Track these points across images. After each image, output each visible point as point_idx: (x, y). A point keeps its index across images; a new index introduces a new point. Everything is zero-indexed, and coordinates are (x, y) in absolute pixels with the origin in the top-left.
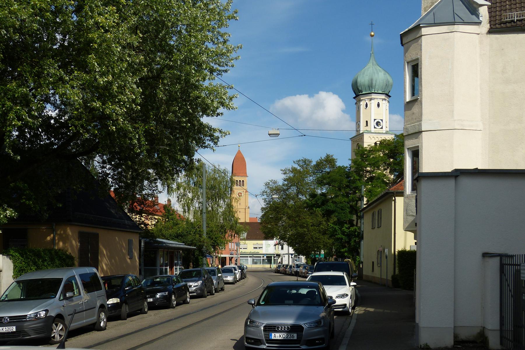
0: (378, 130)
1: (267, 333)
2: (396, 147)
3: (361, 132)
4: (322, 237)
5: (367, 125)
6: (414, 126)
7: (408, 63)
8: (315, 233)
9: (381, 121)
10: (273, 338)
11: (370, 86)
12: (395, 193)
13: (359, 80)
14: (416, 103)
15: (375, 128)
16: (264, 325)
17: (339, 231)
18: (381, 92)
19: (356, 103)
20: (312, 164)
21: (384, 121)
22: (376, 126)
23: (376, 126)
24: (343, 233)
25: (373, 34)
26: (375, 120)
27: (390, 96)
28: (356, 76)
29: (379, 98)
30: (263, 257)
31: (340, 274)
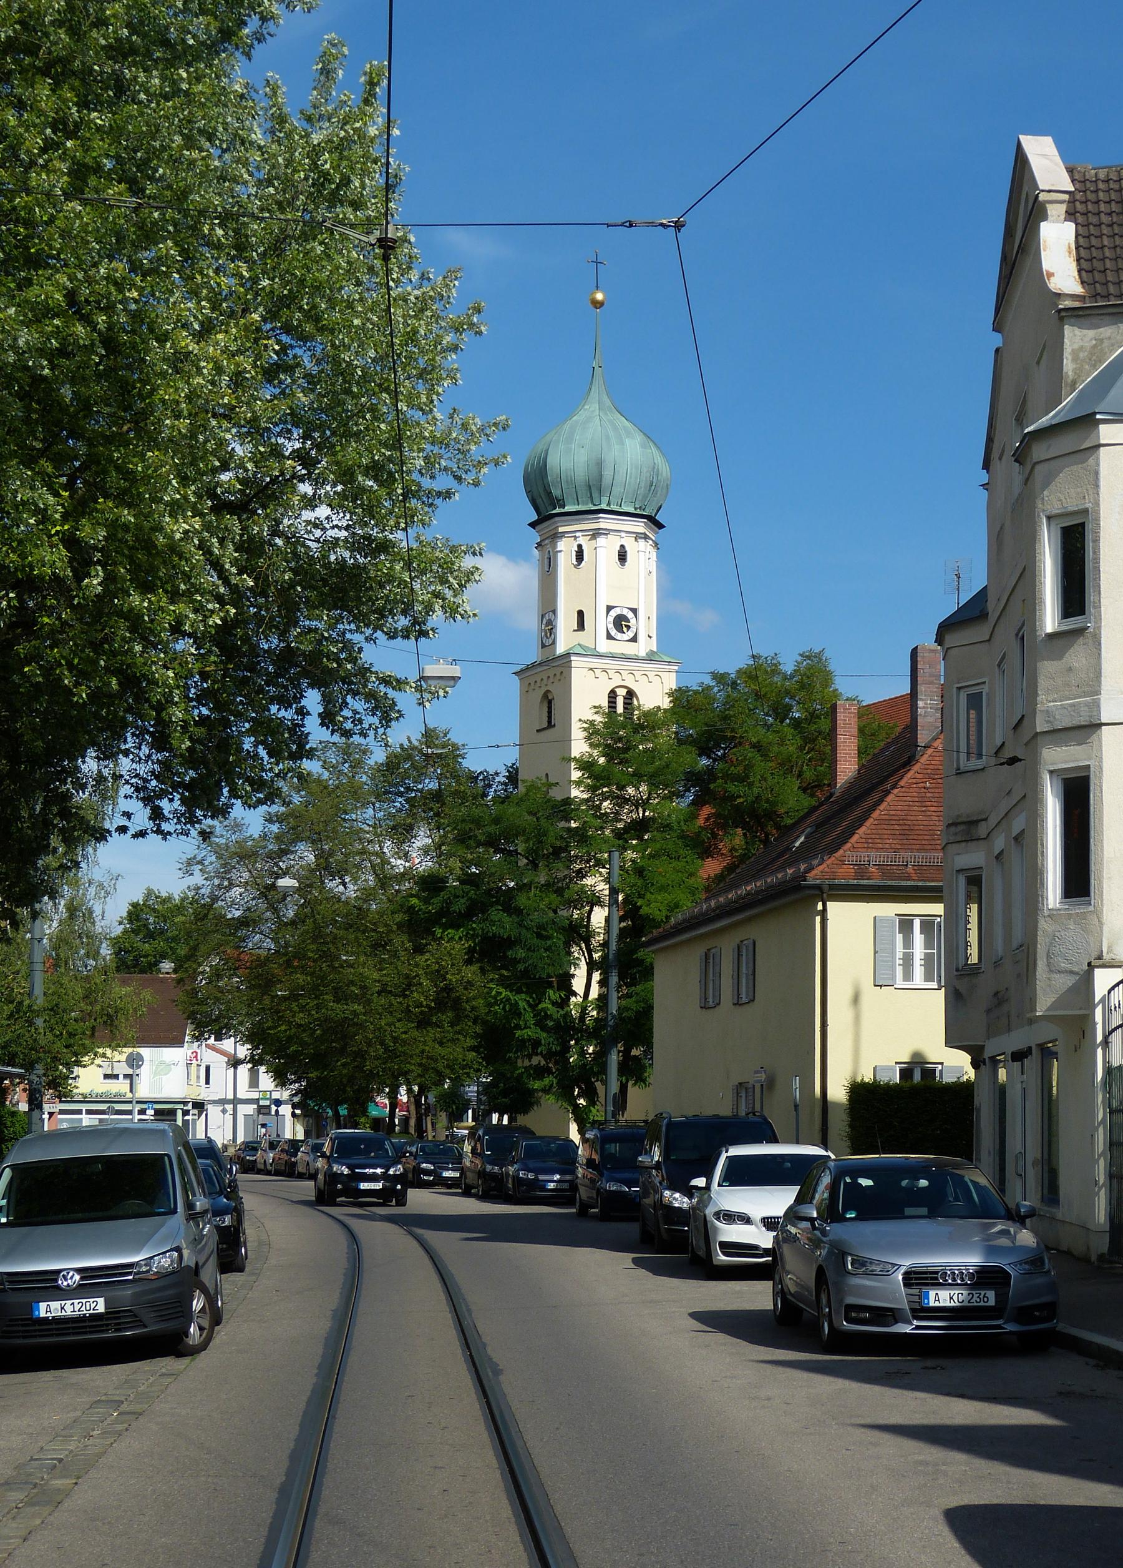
0: (620, 647)
1: (915, 1291)
2: (725, 718)
3: (560, 649)
4: (416, 1033)
5: (581, 626)
6: (1073, 705)
7: (1049, 518)
8: (390, 1019)
9: (630, 615)
10: (932, 1304)
11: (594, 486)
12: (826, 888)
13: (552, 461)
14: (1081, 640)
15: (610, 637)
16: (903, 1270)
17: (529, 1017)
18: (631, 510)
19: (539, 545)
20: (371, 762)
21: (641, 613)
22: (613, 632)
23: (613, 632)
24: (542, 1020)
25: (599, 296)
26: (609, 608)
27: (660, 526)
28: (541, 447)
29: (624, 531)
30: (142, 1112)
31: (724, 1156)
